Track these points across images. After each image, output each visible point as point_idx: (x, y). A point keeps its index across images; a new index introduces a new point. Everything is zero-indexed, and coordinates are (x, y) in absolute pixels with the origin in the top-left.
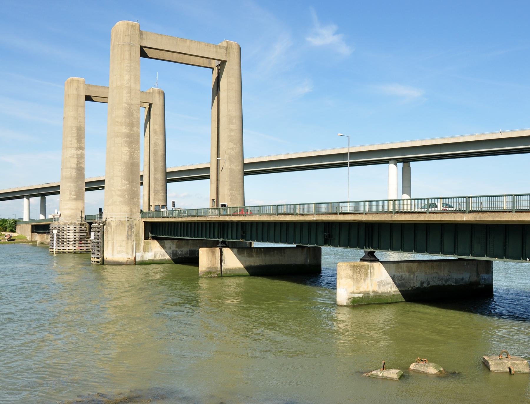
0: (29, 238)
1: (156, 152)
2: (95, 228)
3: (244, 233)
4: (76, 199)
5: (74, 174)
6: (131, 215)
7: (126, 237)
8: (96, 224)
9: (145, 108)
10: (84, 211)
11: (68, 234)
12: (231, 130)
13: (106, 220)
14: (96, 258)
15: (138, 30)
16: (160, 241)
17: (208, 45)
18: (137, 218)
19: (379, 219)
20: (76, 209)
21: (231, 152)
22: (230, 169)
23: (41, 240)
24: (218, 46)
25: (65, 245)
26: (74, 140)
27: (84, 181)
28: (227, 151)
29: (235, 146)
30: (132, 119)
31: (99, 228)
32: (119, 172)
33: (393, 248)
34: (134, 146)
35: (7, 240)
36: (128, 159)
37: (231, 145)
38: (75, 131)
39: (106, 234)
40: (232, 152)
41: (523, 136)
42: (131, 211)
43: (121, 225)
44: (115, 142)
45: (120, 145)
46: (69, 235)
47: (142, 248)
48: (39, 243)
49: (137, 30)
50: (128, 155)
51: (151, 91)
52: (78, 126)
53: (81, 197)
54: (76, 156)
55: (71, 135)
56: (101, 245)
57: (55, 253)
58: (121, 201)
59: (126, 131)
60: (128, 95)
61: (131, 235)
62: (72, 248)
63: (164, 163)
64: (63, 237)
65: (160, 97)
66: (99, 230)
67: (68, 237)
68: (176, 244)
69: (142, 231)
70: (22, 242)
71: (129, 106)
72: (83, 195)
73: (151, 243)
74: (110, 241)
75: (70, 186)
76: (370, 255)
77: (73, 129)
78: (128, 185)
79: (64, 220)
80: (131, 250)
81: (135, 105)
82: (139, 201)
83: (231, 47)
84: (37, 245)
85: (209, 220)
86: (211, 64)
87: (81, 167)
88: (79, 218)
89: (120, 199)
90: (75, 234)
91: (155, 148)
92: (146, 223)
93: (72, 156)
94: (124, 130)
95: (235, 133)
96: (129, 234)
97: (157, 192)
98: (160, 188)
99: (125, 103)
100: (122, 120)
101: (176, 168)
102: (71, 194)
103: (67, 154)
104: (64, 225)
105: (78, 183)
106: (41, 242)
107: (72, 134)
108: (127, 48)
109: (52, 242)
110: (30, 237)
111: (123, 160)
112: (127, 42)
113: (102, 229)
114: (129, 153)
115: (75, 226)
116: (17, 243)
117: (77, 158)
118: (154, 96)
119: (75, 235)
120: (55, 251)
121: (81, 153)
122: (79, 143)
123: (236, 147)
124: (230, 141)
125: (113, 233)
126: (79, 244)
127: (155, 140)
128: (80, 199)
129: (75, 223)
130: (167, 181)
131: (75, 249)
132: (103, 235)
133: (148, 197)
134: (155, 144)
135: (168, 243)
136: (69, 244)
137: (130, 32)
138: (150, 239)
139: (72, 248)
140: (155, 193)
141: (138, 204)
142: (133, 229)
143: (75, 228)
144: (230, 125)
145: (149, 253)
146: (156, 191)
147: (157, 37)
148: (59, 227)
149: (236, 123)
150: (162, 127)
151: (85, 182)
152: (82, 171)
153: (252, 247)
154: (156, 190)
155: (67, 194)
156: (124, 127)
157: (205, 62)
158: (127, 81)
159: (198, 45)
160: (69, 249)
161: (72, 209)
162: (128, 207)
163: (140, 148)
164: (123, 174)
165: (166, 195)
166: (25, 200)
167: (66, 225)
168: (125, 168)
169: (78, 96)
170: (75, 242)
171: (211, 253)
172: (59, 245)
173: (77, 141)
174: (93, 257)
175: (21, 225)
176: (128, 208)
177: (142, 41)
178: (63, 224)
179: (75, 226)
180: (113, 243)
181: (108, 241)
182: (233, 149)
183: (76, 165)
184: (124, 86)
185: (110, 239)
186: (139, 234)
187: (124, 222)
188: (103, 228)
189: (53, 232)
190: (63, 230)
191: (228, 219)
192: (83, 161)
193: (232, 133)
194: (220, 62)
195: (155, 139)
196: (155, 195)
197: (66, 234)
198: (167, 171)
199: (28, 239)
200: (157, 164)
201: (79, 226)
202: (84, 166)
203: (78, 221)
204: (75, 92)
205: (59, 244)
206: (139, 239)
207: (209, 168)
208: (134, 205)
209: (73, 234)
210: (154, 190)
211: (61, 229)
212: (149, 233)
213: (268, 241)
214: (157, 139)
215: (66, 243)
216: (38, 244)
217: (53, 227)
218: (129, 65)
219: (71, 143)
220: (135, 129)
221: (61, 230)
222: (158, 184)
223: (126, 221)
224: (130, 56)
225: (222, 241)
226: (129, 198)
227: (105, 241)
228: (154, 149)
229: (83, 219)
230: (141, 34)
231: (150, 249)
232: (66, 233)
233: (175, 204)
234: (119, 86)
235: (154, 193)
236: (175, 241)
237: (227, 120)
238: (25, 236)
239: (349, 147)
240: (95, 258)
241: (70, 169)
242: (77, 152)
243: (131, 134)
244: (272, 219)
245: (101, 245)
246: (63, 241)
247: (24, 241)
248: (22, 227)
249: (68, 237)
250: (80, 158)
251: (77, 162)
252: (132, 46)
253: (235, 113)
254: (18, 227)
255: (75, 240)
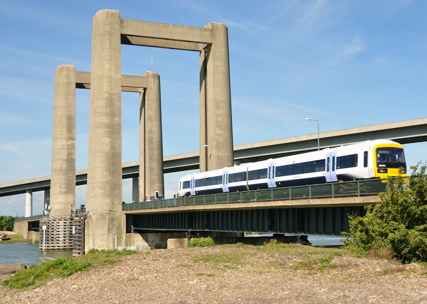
0: (25, 236)
1: (151, 139)
2: (76, 222)
3: (208, 222)
4: (67, 193)
5: (64, 166)
6: (112, 208)
7: (107, 230)
8: (78, 218)
9: (140, 93)
10: (75, 205)
11: (58, 230)
12: (218, 116)
13: (88, 214)
14: (77, 253)
15: (118, 18)
16: (143, 234)
17: (192, 29)
18: (119, 210)
19: (300, 204)
20: (67, 203)
21: (219, 139)
22: (217, 156)
23: (37, 238)
24: (203, 29)
25: (55, 242)
26: (65, 130)
27: (75, 173)
28: (214, 138)
29: (222, 132)
30: (113, 109)
31: (80, 222)
32: (101, 163)
33: (319, 232)
34: (115, 136)
35: (1, 240)
36: (109, 150)
37: (219, 131)
38: (65, 121)
39: (87, 228)
40: (220, 138)
41: (357, 133)
42: (113, 204)
43: (102, 218)
44: (96, 133)
45: (101, 136)
46: (58, 231)
47: (123, 241)
48: (34, 241)
49: (117, 19)
50: (109, 146)
51: (146, 75)
52: (69, 115)
53: (72, 190)
54: (66, 147)
55: (61, 125)
56: (82, 239)
57: (44, 250)
58: (102, 194)
59: (106, 121)
60: (109, 84)
61: (112, 229)
62: (61, 244)
63: (160, 151)
64: (52, 233)
65: (154, 81)
66: (80, 224)
67: (58, 233)
68: (160, 236)
69: (124, 224)
70: (17, 241)
71: (110, 96)
72: (75, 188)
73: (133, 237)
74: (91, 235)
75: (60, 179)
76: (302, 239)
77: (63, 119)
78: (109, 176)
79: (54, 215)
80: (112, 244)
81: (116, 94)
82: (121, 192)
83: (216, 29)
84: (32, 243)
85: (177, 210)
86: (197, 47)
87: (71, 158)
88: (69, 213)
89: (101, 191)
90: (65, 230)
91: (150, 136)
92: (127, 215)
93: (63, 147)
94: (105, 120)
95: (223, 118)
96: (111, 227)
97: (152, 183)
98: (156, 177)
99: (106, 93)
100: (103, 110)
101: (266, 142)
102: (61, 187)
103: (57, 145)
104: (53, 220)
105: (68, 176)
106: (36, 240)
107: (62, 124)
108: (107, 37)
109: (41, 239)
110: (27, 235)
111: (104, 151)
112: (107, 31)
113: (83, 223)
114: (109, 144)
115: (65, 221)
116: (11, 243)
117: (68, 149)
118: (148, 80)
119: (65, 231)
120: (44, 248)
121: (72, 143)
122: (69, 133)
123: (224, 133)
124: (217, 126)
125: (94, 227)
126: (69, 240)
127: (150, 127)
128: (71, 193)
129: (65, 218)
130: (164, 171)
131: (65, 246)
132: (84, 229)
133: (144, 188)
134: (150, 131)
135: (151, 237)
136: (58, 240)
137: (110, 20)
138: (133, 233)
139: (61, 244)
140: (150, 183)
141: (119, 196)
142: (114, 222)
143: (65, 223)
144: (217, 110)
145: (131, 247)
146: (152, 182)
147: (138, 24)
148: (49, 223)
149: (223, 107)
150: (157, 112)
151: (123, 167)
152: (72, 162)
153: (245, 237)
154: (151, 180)
155: (57, 188)
156: (105, 117)
157: (192, 46)
158: (108, 70)
159: (182, 29)
160: (58, 246)
161: (62, 203)
162: (110, 199)
163: (121, 138)
164: (104, 166)
165: (162, 185)
166: (28, 195)
167: (56, 220)
168: (106, 159)
169: (68, 84)
170: (65, 239)
171: (179, 244)
172: (48, 242)
173: (68, 132)
174: (74, 253)
175: (19, 222)
176: (110, 201)
177: (123, 28)
178: (52, 219)
179: (65, 221)
180: (94, 237)
181: (89, 235)
182: (220, 135)
183: (66, 156)
184: (105, 76)
185: (91, 233)
186: (121, 227)
187: (105, 214)
188: (84, 222)
189: (42, 229)
190: (53, 226)
191: (191, 209)
192: (74, 152)
193: (220, 119)
194: (207, 44)
195: (150, 126)
196: (151, 186)
197: (55, 230)
198: (164, 160)
199: (25, 238)
200: (152, 152)
201: (69, 221)
202: (75, 158)
203: (68, 216)
204: (65, 80)
205: (48, 240)
206: (120, 233)
207: (198, 157)
208: (115, 197)
209: (62, 230)
210: (149, 181)
211: (51, 224)
212: (132, 226)
213: (317, 233)
214: (152, 125)
215: (56, 240)
216: (33, 243)
217: (42, 223)
218: (109, 54)
219: (61, 133)
220: (116, 119)
221: (50, 226)
222: (154, 173)
223: (107, 214)
224: (111, 45)
225: (191, 231)
226: (110, 190)
227: (86, 235)
228: (149, 137)
229: (74, 213)
230: (122, 21)
231: (132, 243)
232: (56, 228)
233: (158, 195)
234: (100, 76)
235: (149, 184)
236: (159, 233)
237: (214, 105)
238: (22, 235)
239: (319, 133)
240: (76, 253)
241: (60, 161)
242: (67, 143)
243: (112, 124)
244: (224, 207)
245: (82, 239)
246: (53, 237)
247: (19, 240)
248: (20, 225)
249: (58, 233)
250: (71, 148)
251: (67, 154)
252: (112, 35)
253: (222, 96)
254: (16, 225)
255: (65, 236)
